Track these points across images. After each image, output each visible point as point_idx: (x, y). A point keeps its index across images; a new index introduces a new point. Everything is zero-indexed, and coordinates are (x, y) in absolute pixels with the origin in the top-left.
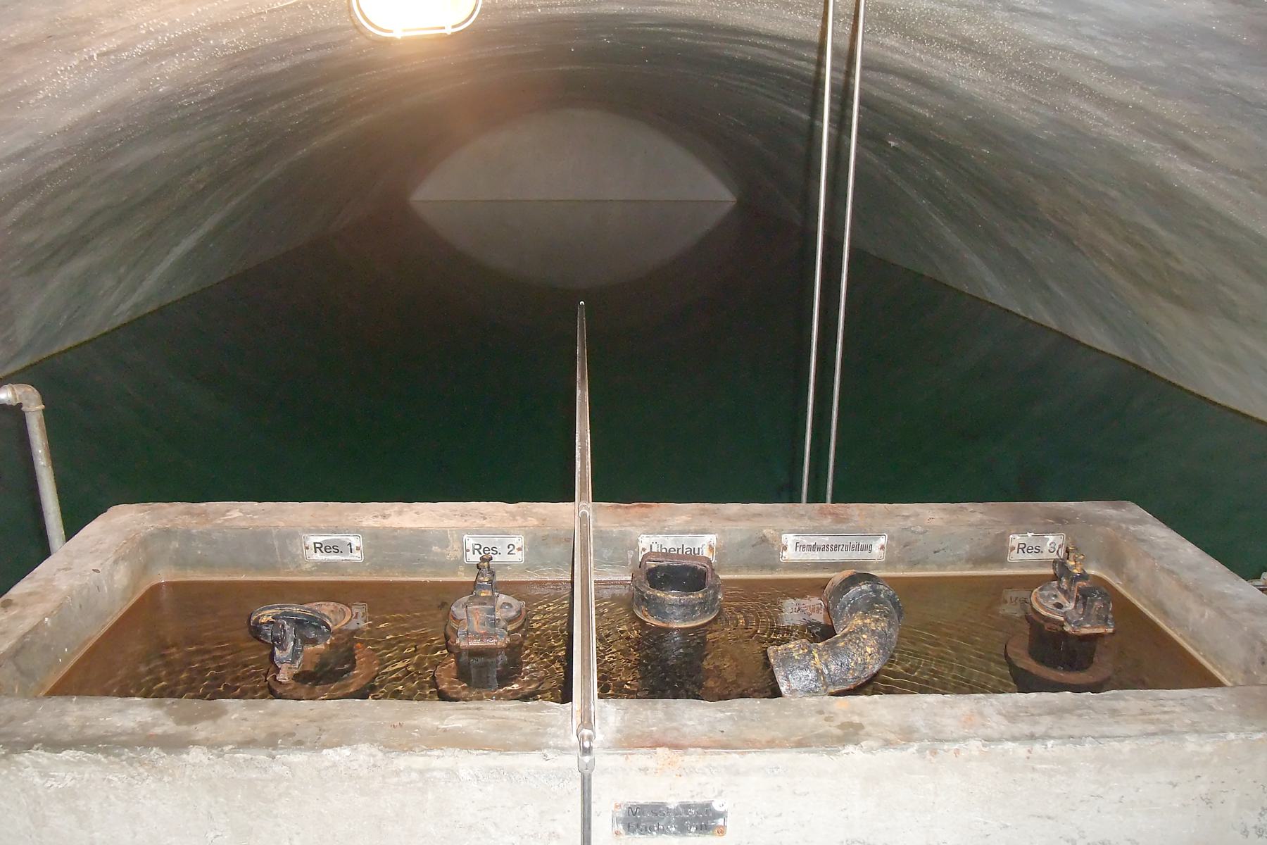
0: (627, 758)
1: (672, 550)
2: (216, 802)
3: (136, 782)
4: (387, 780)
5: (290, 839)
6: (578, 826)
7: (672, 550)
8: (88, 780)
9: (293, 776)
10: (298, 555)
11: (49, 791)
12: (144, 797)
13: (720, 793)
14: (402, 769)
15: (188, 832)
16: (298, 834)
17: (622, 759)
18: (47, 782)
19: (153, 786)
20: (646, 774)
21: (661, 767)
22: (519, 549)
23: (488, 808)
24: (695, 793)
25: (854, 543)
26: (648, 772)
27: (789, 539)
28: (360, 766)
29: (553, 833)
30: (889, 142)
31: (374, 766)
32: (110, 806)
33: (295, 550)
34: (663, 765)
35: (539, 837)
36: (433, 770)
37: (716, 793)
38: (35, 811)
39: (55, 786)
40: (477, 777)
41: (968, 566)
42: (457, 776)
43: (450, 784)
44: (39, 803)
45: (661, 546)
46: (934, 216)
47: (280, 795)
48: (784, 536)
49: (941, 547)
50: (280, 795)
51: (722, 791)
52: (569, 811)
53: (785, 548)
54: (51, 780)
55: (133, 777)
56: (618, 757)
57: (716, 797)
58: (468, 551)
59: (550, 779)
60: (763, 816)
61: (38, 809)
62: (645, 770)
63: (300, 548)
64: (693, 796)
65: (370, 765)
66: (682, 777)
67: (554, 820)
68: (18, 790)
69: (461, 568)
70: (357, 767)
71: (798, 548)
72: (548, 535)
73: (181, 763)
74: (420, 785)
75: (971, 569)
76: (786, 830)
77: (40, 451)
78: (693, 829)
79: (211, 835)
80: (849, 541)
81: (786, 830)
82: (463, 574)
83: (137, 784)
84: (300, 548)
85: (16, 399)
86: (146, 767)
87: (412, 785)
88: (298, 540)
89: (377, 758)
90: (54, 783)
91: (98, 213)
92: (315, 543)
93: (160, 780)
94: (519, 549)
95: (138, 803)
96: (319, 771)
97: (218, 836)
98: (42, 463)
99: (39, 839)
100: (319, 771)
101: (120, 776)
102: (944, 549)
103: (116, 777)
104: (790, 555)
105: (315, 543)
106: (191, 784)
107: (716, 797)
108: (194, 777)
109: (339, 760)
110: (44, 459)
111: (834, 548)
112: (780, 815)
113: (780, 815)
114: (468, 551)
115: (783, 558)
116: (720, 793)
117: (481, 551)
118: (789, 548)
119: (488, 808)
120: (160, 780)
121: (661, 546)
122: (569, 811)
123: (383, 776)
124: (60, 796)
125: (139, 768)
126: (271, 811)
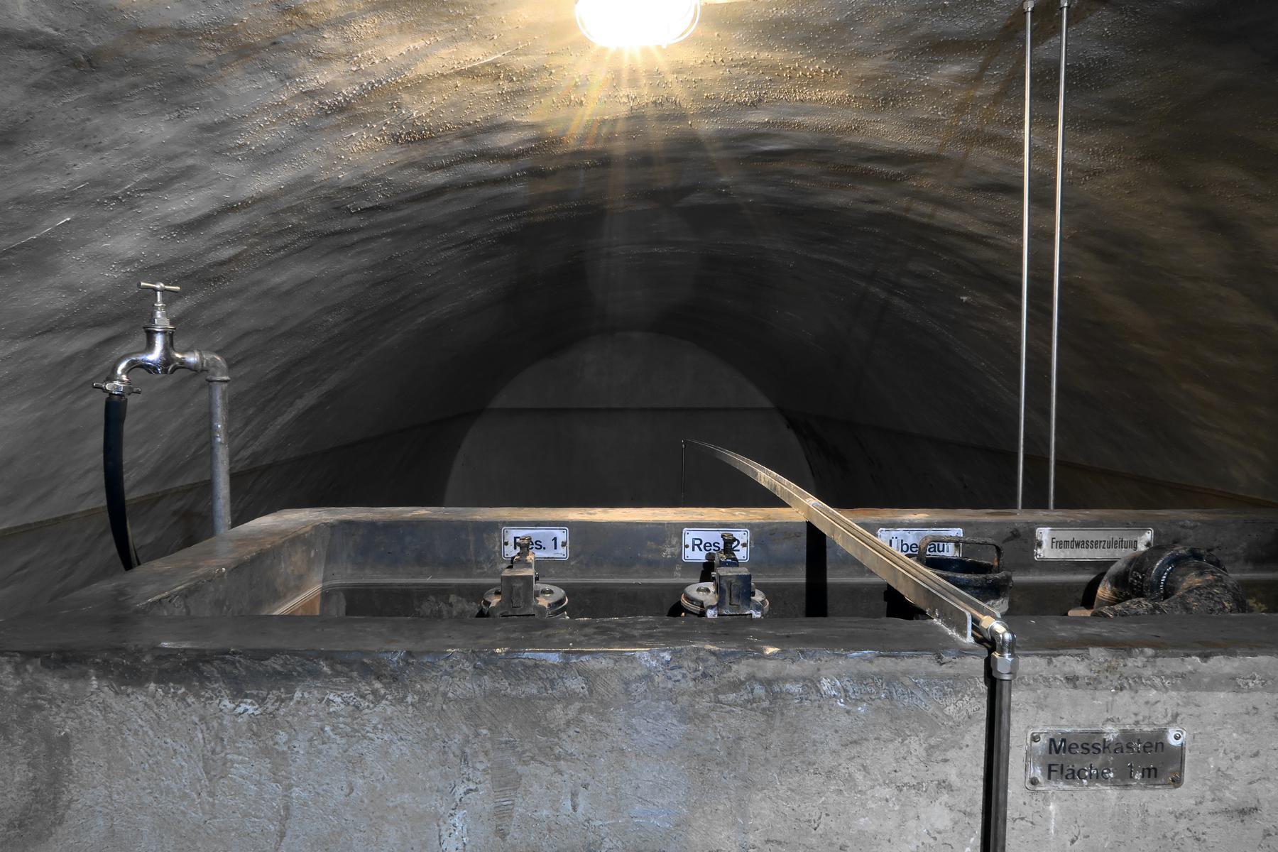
0: (1050, 662)
1: (914, 546)
2: (477, 735)
3: (367, 704)
4: (721, 697)
5: (573, 794)
6: (978, 771)
7: (914, 546)
8: (299, 702)
9: (591, 692)
10: (495, 553)
11: (240, 720)
12: (375, 727)
13: (1175, 716)
14: (743, 679)
15: (428, 785)
16: (585, 787)
17: (1042, 662)
18: (238, 706)
19: (389, 711)
20: (1075, 687)
21: (1095, 675)
22: (744, 545)
23: (855, 742)
24: (1140, 718)
25: (1116, 538)
26: (1077, 683)
27: (1044, 534)
28: (684, 676)
29: (944, 782)
30: (961, 298)
31: (705, 675)
32: (324, 743)
33: (491, 546)
34: (1099, 672)
35: (924, 789)
36: (785, 680)
37: (1169, 718)
38: (213, 752)
39: (250, 712)
40: (846, 691)
41: (1248, 567)
42: (818, 691)
43: (806, 703)
44: (222, 740)
45: (902, 541)
46: (993, 379)
47: (568, 724)
48: (1039, 530)
49: (1215, 544)
50: (568, 724)
51: (1177, 715)
52: (967, 746)
53: (1040, 545)
54: (246, 703)
55: (363, 697)
56: (1037, 659)
57: (1168, 723)
58: (687, 546)
59: (944, 694)
60: (1232, 755)
61: (218, 749)
62: (1072, 680)
63: (498, 544)
64: (1137, 723)
65: (699, 674)
66: (1125, 691)
67: (946, 761)
68: (196, 719)
69: (678, 568)
70: (679, 677)
71: (1054, 544)
72: (776, 529)
73: (435, 674)
74: (766, 704)
75: (1251, 571)
76: (1264, 778)
77: (219, 426)
78: (1138, 776)
79: (461, 790)
80: (1111, 537)
81: (1264, 778)
82: (680, 575)
83: (368, 707)
84: (498, 544)
85: (203, 364)
86: (385, 680)
87: (755, 705)
88: (496, 535)
89: (709, 663)
90: (248, 707)
91: (247, 334)
92: (515, 538)
93: (402, 700)
94: (744, 545)
95: (364, 737)
96: (627, 683)
97: (471, 790)
98: (219, 440)
99: (211, 800)
100: (627, 683)
101: (345, 695)
102: (1218, 547)
103: (339, 696)
104: (1045, 552)
105: (515, 538)
106: (444, 707)
107: (1168, 723)
108: (450, 695)
109: (656, 667)
110: (223, 436)
111: (1095, 544)
112: (1256, 755)
113: (1256, 755)
114: (687, 546)
115: (1038, 557)
116: (1175, 716)
117: (702, 546)
118: (1044, 545)
119: (855, 742)
120: (402, 700)
121: (902, 541)
122: (967, 746)
123: (716, 691)
124: (255, 728)
125: (374, 682)
126: (552, 749)
